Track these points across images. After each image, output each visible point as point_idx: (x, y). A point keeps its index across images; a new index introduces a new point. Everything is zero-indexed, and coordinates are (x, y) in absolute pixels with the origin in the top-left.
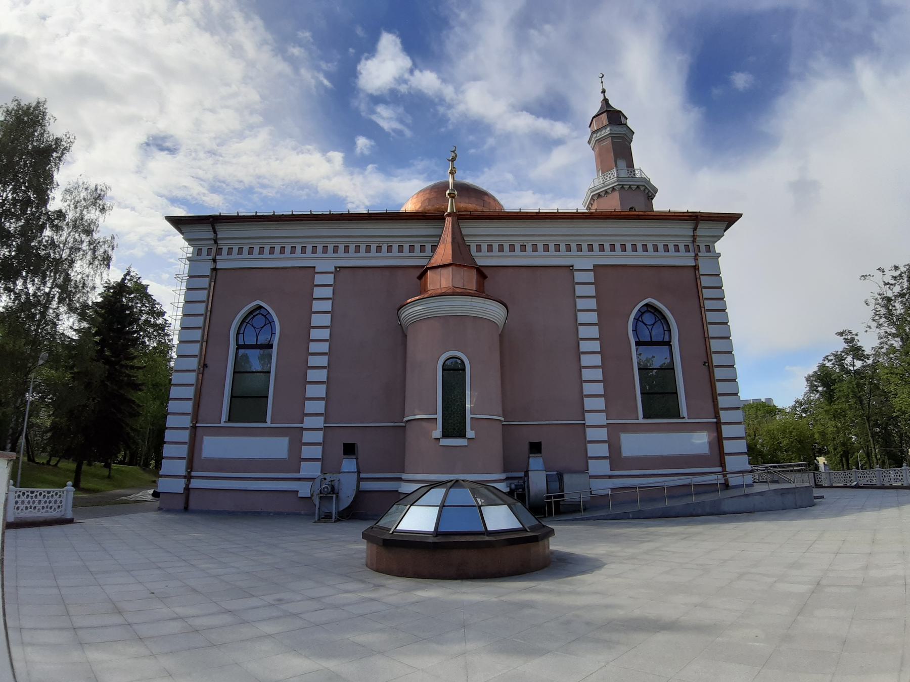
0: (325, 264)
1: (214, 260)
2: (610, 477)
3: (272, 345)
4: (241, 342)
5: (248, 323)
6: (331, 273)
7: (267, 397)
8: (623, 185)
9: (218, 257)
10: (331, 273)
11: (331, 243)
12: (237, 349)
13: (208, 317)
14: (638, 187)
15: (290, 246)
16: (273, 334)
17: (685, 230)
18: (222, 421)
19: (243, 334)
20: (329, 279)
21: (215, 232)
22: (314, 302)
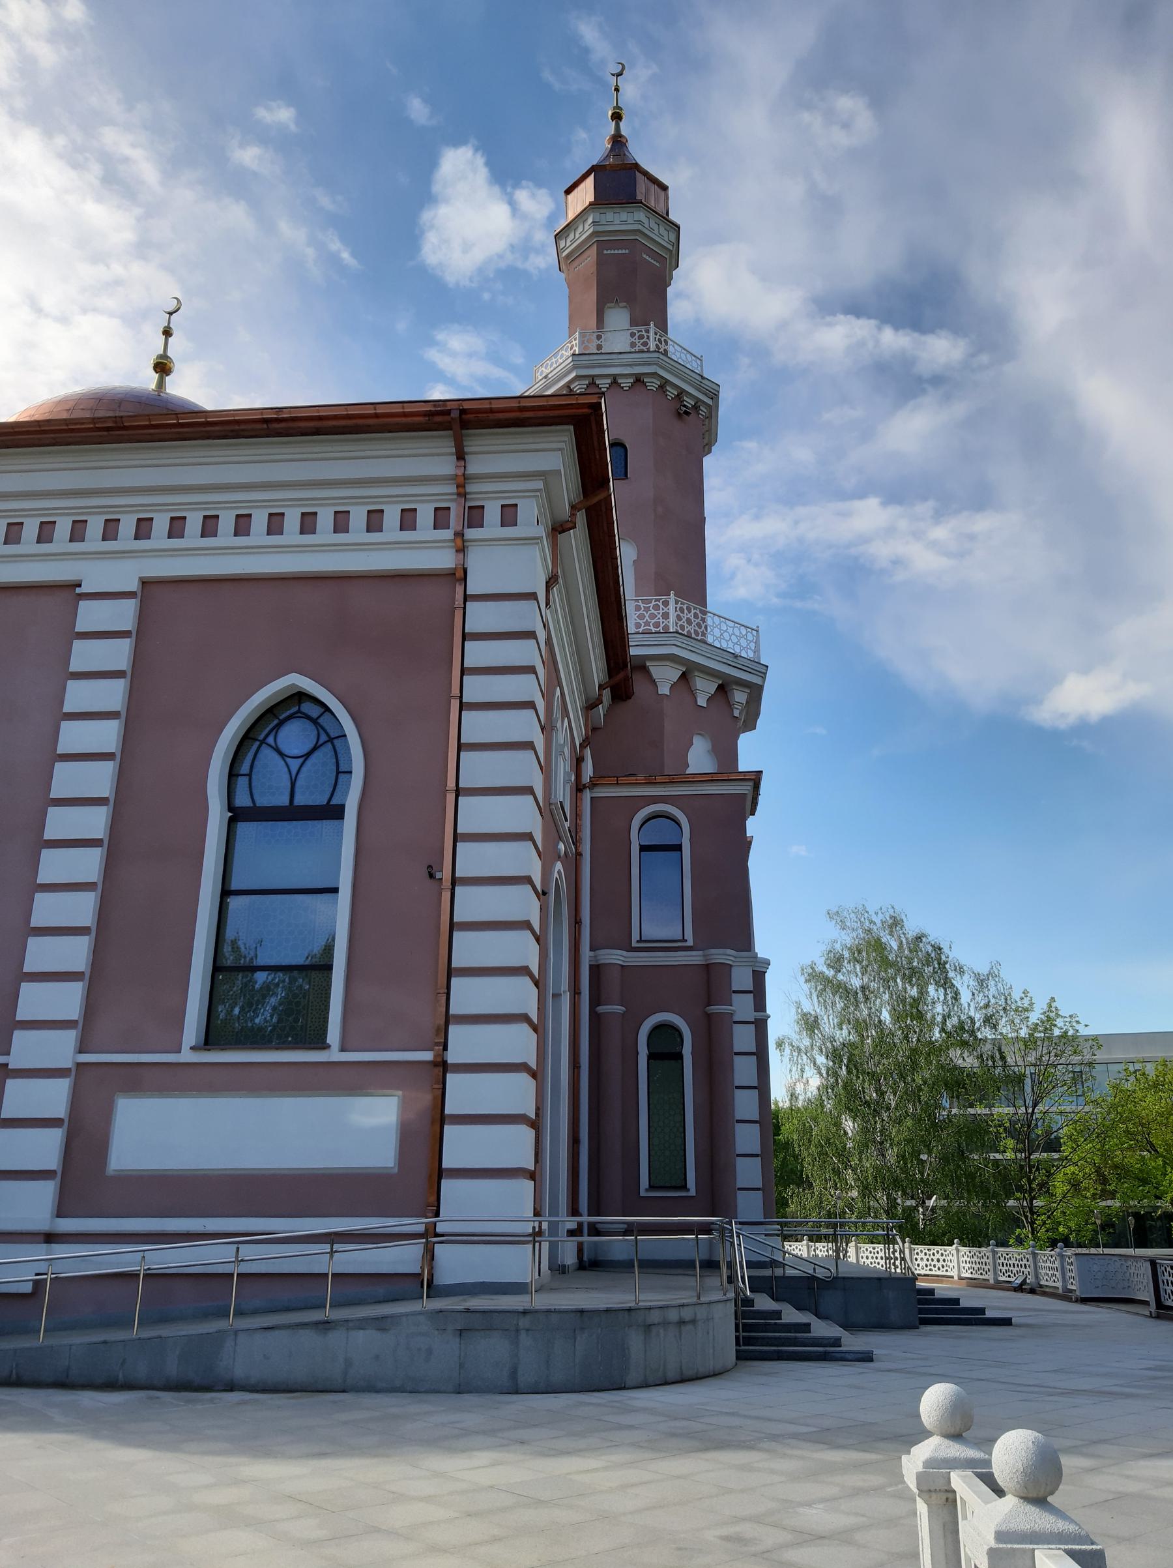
2: (50, 1238)
3: (341, 808)
4: (242, 800)
8: (593, 377)
12: (232, 821)
14: (639, 380)
16: (341, 772)
18: (185, 1047)
19: (250, 775)
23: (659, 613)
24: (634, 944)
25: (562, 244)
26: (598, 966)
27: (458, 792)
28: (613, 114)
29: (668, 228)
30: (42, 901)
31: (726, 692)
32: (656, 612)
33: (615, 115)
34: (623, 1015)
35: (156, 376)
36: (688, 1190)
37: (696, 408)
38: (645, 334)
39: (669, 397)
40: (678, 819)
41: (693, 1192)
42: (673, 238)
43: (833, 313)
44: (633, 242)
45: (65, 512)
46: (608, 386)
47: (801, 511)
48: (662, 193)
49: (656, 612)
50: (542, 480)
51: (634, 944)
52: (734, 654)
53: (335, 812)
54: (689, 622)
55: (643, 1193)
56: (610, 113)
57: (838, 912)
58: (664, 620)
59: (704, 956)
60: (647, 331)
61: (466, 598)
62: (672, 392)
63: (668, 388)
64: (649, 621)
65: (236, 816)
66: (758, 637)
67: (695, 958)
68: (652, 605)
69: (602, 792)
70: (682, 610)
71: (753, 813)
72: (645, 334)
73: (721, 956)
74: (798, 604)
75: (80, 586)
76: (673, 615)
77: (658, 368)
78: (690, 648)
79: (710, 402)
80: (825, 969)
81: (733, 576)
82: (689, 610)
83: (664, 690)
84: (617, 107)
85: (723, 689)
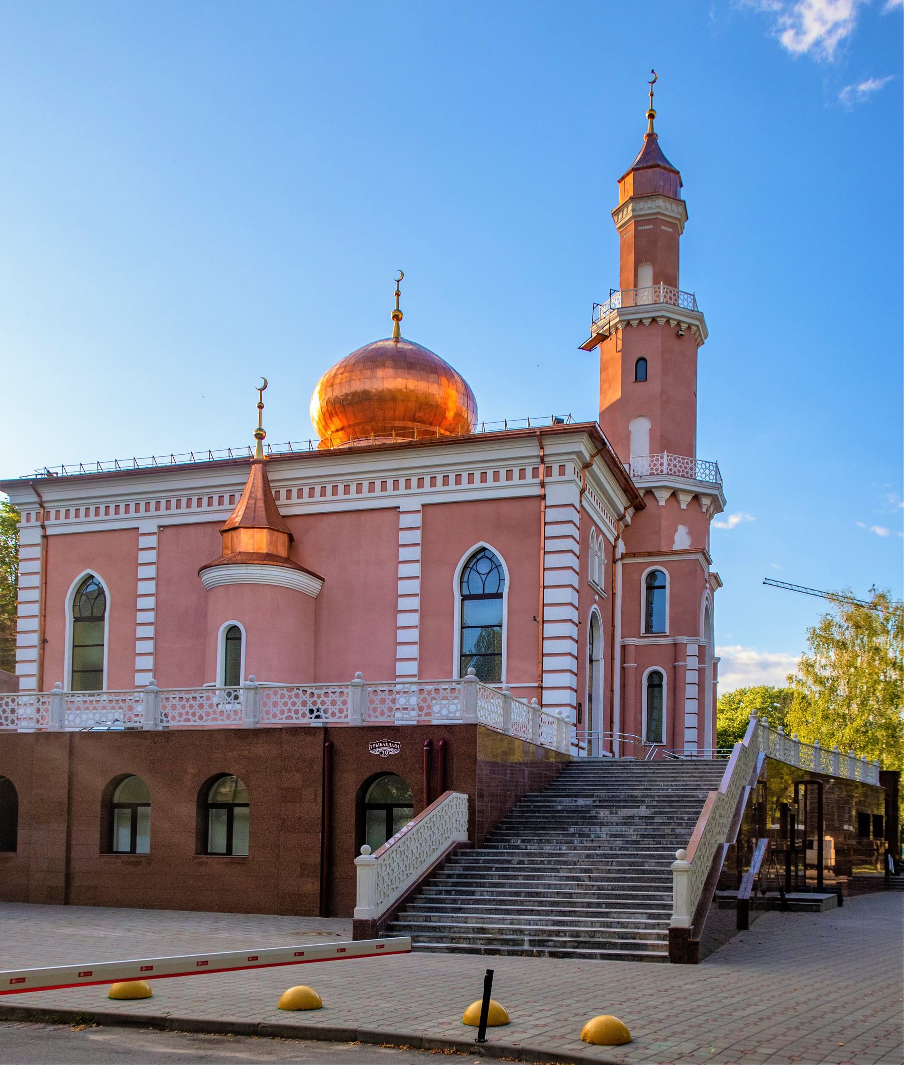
0: (149, 526)
1: (43, 527)
4: (466, 592)
5: (471, 568)
6: (154, 534)
7: (102, 671)
9: (47, 523)
10: (154, 534)
11: (216, 493)
12: (463, 600)
13: (44, 589)
14: (654, 320)
15: (331, 485)
16: (501, 580)
17: (531, 450)
20: (152, 541)
21: (39, 496)
22: (139, 568)
26: (624, 646)
27: (544, 587)
30: (400, 633)
34: (636, 668)
35: (395, 322)
41: (665, 744)
42: (681, 209)
44: (655, 220)
45: (390, 477)
48: (677, 176)
53: (499, 596)
54: (675, 466)
56: (647, 115)
60: (659, 288)
61: (546, 507)
62: (673, 323)
65: (465, 598)
67: (669, 641)
69: (627, 561)
70: (671, 460)
73: (683, 639)
75: (399, 507)
76: (665, 465)
82: (675, 459)
83: (662, 503)
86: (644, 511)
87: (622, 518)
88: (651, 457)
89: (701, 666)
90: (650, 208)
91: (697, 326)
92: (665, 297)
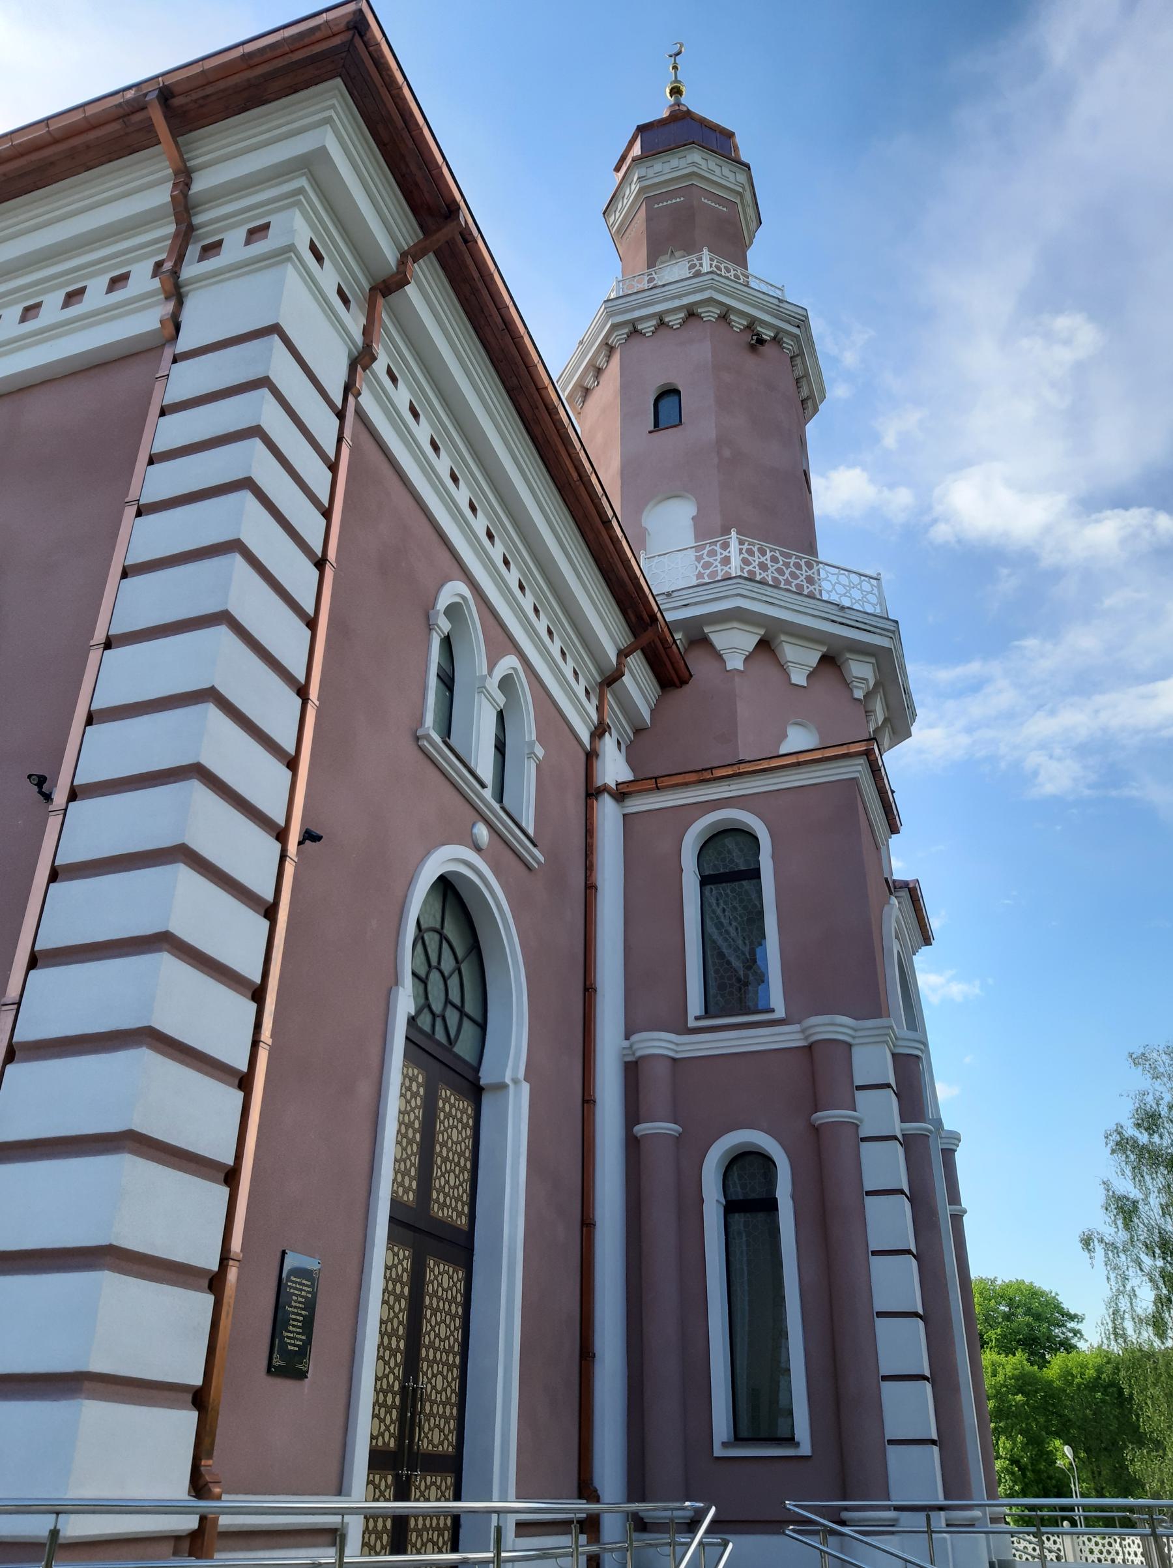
8: (633, 323)
14: (691, 314)
23: (716, 566)
24: (692, 1023)
25: (612, 219)
28: (671, 91)
29: (734, 169)
31: (839, 666)
32: (711, 560)
33: (675, 90)
34: (678, 1139)
36: (797, 1445)
37: (777, 340)
38: (697, 263)
39: (735, 328)
40: (748, 825)
41: (805, 1449)
43: (1099, 510)
46: (653, 328)
47: (1100, 699)
49: (711, 560)
50: (304, 174)
51: (692, 1023)
52: (838, 605)
55: (718, 1451)
56: (668, 91)
57: (1144, 1054)
58: (723, 567)
59: (803, 1031)
62: (739, 323)
63: (732, 317)
64: (703, 571)
66: (879, 587)
67: (788, 1037)
68: (705, 552)
69: (639, 804)
70: (750, 552)
71: (894, 829)
72: (697, 263)
74: (1114, 793)
77: (713, 292)
78: (765, 598)
79: (796, 331)
80: (1137, 1134)
81: (1036, 774)
83: (735, 662)
84: (676, 81)
85: (830, 661)
86: (686, 689)
87: (610, 680)
88: (698, 548)
89: (913, 1127)
90: (676, 169)
91: (796, 336)
92: (746, 562)
